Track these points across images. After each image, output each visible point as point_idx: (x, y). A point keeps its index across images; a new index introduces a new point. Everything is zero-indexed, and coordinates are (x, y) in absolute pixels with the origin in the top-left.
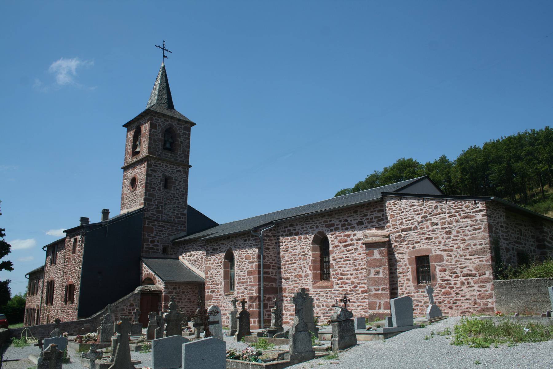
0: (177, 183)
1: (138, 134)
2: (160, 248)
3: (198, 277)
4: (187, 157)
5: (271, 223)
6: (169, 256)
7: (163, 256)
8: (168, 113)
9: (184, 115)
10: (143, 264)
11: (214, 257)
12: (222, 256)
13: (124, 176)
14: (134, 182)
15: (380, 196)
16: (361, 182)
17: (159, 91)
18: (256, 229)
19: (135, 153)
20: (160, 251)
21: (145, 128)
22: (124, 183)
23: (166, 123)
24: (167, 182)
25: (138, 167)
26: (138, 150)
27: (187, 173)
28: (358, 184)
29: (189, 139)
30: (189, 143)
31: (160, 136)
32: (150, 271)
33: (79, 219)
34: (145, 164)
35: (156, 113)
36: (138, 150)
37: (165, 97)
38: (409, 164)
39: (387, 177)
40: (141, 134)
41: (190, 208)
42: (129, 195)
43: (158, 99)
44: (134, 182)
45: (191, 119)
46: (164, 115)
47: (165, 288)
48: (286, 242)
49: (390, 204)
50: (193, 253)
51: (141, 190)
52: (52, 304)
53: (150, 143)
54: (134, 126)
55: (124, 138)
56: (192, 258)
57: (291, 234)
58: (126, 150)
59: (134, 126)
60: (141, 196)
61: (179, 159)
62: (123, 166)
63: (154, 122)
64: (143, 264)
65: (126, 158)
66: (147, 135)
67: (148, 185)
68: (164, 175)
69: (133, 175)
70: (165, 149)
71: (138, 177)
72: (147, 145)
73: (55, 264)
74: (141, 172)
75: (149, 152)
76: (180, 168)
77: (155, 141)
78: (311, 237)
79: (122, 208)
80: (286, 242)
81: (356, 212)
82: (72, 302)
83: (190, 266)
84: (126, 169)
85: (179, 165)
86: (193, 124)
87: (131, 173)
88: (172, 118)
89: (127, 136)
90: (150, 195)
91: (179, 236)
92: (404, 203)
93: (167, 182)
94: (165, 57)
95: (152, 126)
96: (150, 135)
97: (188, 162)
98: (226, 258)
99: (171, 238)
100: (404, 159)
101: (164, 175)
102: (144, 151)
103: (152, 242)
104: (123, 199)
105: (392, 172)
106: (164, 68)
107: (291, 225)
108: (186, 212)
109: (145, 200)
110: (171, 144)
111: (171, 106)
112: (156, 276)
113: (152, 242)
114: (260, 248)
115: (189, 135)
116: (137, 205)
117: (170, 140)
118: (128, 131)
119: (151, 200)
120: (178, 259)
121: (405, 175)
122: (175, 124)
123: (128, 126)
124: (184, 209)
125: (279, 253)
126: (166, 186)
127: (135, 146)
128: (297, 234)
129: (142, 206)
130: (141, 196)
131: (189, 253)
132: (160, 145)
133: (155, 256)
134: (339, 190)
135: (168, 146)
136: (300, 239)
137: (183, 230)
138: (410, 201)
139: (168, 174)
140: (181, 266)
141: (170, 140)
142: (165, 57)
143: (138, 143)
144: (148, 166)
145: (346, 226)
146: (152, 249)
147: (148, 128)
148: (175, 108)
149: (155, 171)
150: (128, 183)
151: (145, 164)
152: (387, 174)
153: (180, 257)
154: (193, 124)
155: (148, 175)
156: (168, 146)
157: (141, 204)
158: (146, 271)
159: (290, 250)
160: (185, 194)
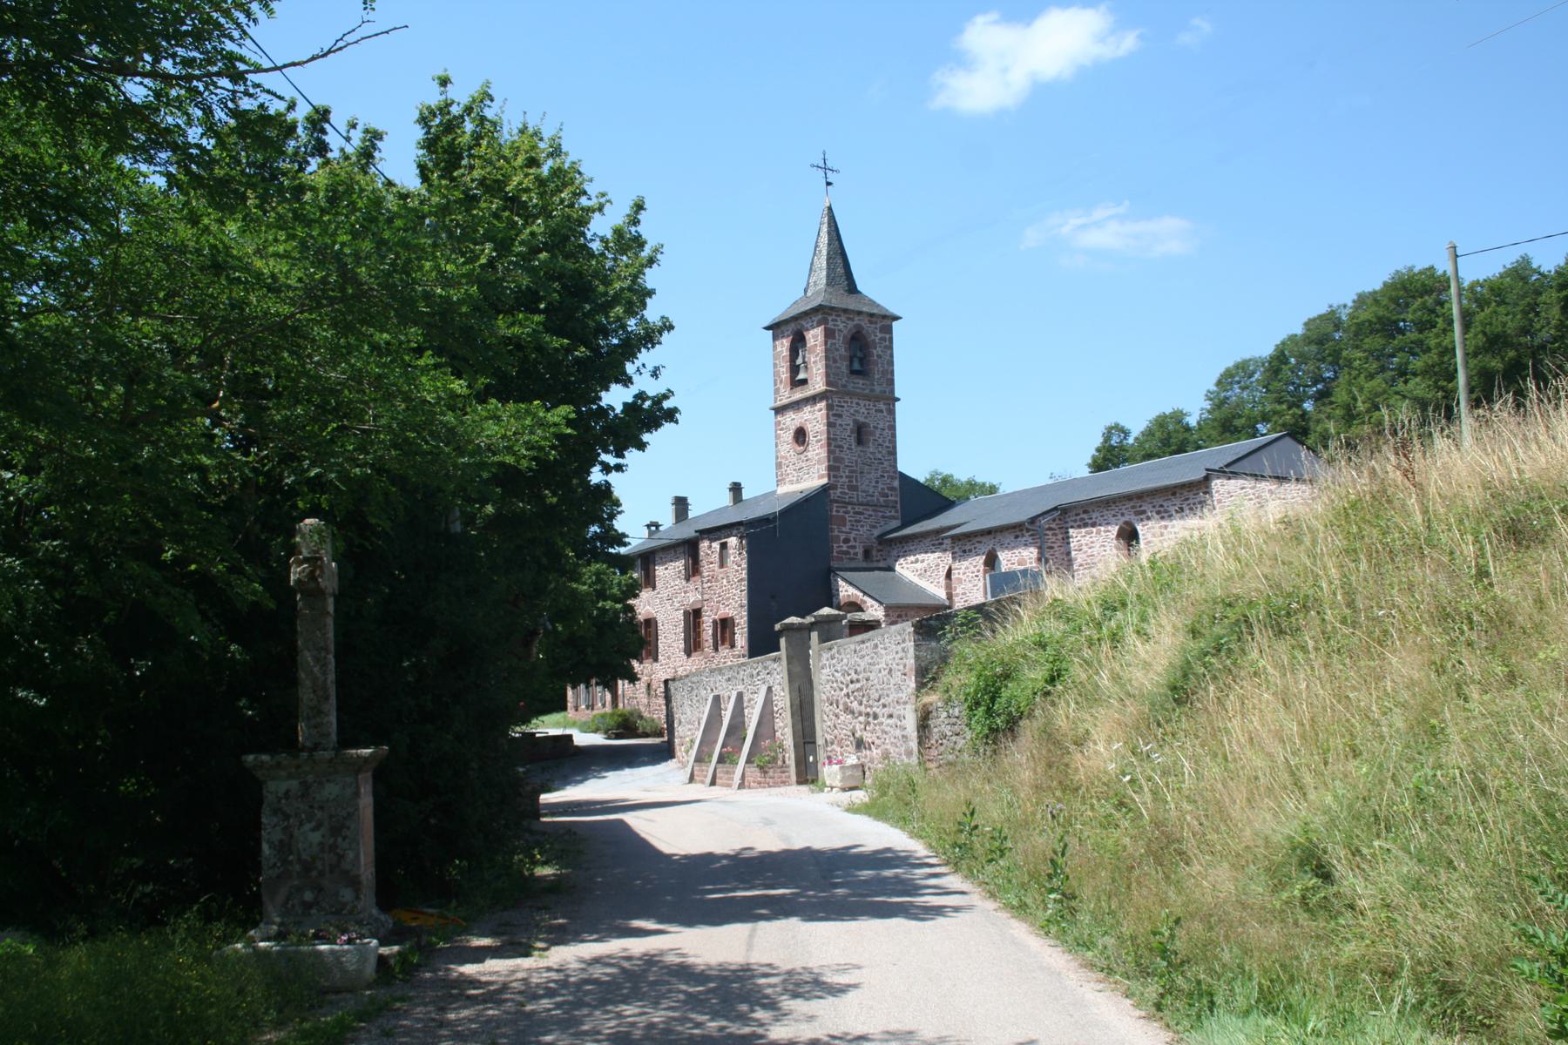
0: (878, 432)
1: (798, 342)
2: (860, 550)
3: (933, 597)
4: (891, 382)
5: (1055, 509)
6: (875, 565)
7: (864, 565)
8: (850, 303)
9: (878, 301)
10: (841, 582)
11: (966, 563)
12: (981, 560)
13: (778, 424)
14: (800, 435)
15: (1204, 473)
16: (1292, 338)
17: (829, 259)
18: (1033, 520)
19: (797, 383)
20: (860, 556)
21: (815, 336)
22: (777, 437)
23: (851, 324)
24: (861, 433)
25: (808, 409)
26: (801, 376)
27: (892, 412)
28: (1283, 343)
29: (891, 347)
30: (892, 356)
31: (843, 351)
32: (852, 591)
33: (670, 500)
34: (823, 405)
35: (832, 308)
36: (801, 376)
37: (840, 270)
38: (1423, 285)
39: (1363, 323)
40: (804, 345)
41: (903, 477)
42: (794, 459)
43: (828, 276)
44: (800, 435)
45: (893, 309)
46: (845, 311)
47: (886, 616)
48: (1078, 537)
49: (1217, 484)
50: (920, 557)
51: (817, 450)
52: (656, 660)
53: (827, 366)
54: (790, 329)
55: (769, 354)
56: (918, 566)
57: (1085, 525)
58: (776, 374)
59: (790, 329)
60: (819, 462)
61: (878, 388)
62: (773, 405)
63: (830, 325)
64: (841, 582)
65: (777, 391)
66: (820, 350)
67: (833, 444)
68: (855, 421)
69: (797, 423)
70: (853, 372)
71: (809, 428)
72: (822, 370)
73: (654, 588)
74: (815, 419)
75: (828, 383)
76: (882, 406)
77: (835, 361)
78: (1115, 529)
79: (779, 482)
80: (1078, 537)
81: (1174, 494)
82: (733, 646)
83: (916, 580)
84: (779, 410)
85: (878, 399)
86: (897, 318)
87: (792, 420)
88: (860, 313)
89: (775, 347)
90: (836, 459)
91: (888, 528)
92: (1233, 485)
93: (861, 433)
94: (829, 184)
95: (829, 334)
96: (826, 350)
97: (893, 391)
98: (986, 563)
99: (876, 532)
100: (1411, 269)
101: (855, 421)
102: (818, 384)
103: (846, 541)
104: (779, 466)
105: (1374, 309)
106: (830, 209)
107: (1085, 512)
108: (896, 484)
109: (830, 468)
110: (861, 360)
111: (852, 289)
112: (866, 598)
113: (846, 541)
114: (1040, 548)
115: (891, 340)
116: (810, 476)
117: (859, 354)
118: (775, 338)
119: (837, 469)
120: (893, 570)
121: (1410, 316)
122: (865, 323)
123: (776, 328)
124: (893, 478)
125: (1069, 553)
126: (860, 442)
127: (794, 369)
128: (1093, 525)
129: (825, 481)
130: (819, 462)
131: (912, 558)
132: (844, 366)
133: (853, 565)
134: (1230, 364)
135: (856, 366)
136: (1099, 532)
137: (894, 518)
138: (1240, 482)
139: (862, 419)
140: (900, 581)
141: (859, 354)
142: (829, 184)
143: (799, 361)
144: (829, 408)
145: (1164, 514)
146: (847, 553)
147: (821, 338)
148: (859, 288)
149: (840, 416)
150: (788, 436)
151: (823, 405)
152: (1364, 316)
153: (897, 568)
154: (897, 318)
155: (830, 425)
156: (856, 366)
157: (821, 477)
158: (846, 591)
159: (1085, 548)
160: (892, 452)
